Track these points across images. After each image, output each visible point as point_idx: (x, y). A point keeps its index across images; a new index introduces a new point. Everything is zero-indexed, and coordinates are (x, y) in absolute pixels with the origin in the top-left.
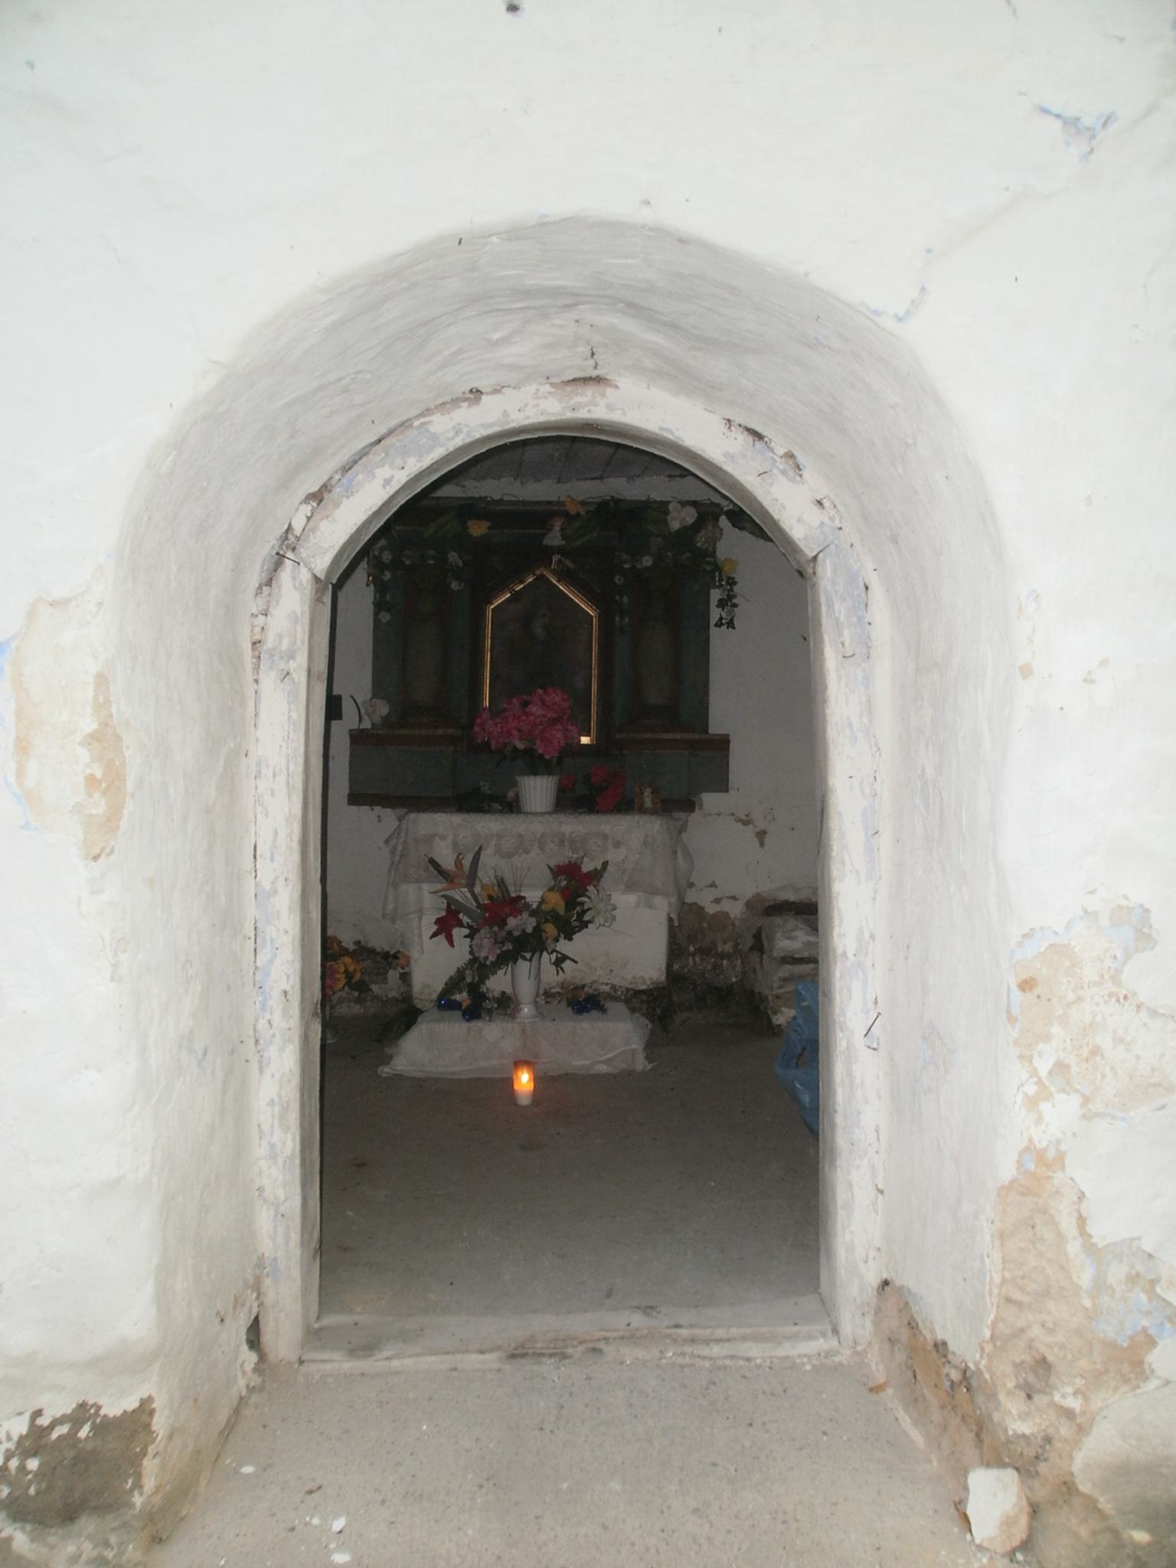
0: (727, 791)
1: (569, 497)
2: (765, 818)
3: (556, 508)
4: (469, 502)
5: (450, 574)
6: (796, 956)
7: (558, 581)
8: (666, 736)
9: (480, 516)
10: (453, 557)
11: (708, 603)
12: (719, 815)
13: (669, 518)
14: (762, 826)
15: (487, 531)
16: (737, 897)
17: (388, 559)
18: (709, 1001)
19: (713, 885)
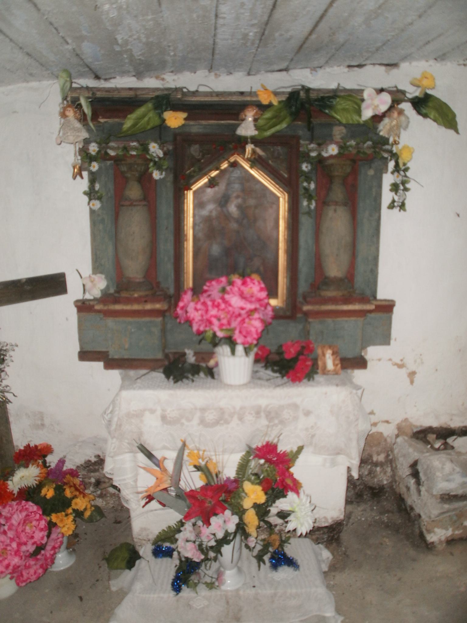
0: (389, 344)
1: (263, 86)
2: (415, 361)
3: (248, 99)
4: (166, 92)
5: (151, 164)
6: (452, 494)
7: (251, 167)
8: (346, 307)
9: (176, 107)
10: (155, 149)
11: (380, 186)
12: (380, 360)
13: (364, 105)
14: (412, 367)
15: (183, 122)
16: (390, 421)
17: (94, 151)
18: (365, 497)
19: (372, 413)
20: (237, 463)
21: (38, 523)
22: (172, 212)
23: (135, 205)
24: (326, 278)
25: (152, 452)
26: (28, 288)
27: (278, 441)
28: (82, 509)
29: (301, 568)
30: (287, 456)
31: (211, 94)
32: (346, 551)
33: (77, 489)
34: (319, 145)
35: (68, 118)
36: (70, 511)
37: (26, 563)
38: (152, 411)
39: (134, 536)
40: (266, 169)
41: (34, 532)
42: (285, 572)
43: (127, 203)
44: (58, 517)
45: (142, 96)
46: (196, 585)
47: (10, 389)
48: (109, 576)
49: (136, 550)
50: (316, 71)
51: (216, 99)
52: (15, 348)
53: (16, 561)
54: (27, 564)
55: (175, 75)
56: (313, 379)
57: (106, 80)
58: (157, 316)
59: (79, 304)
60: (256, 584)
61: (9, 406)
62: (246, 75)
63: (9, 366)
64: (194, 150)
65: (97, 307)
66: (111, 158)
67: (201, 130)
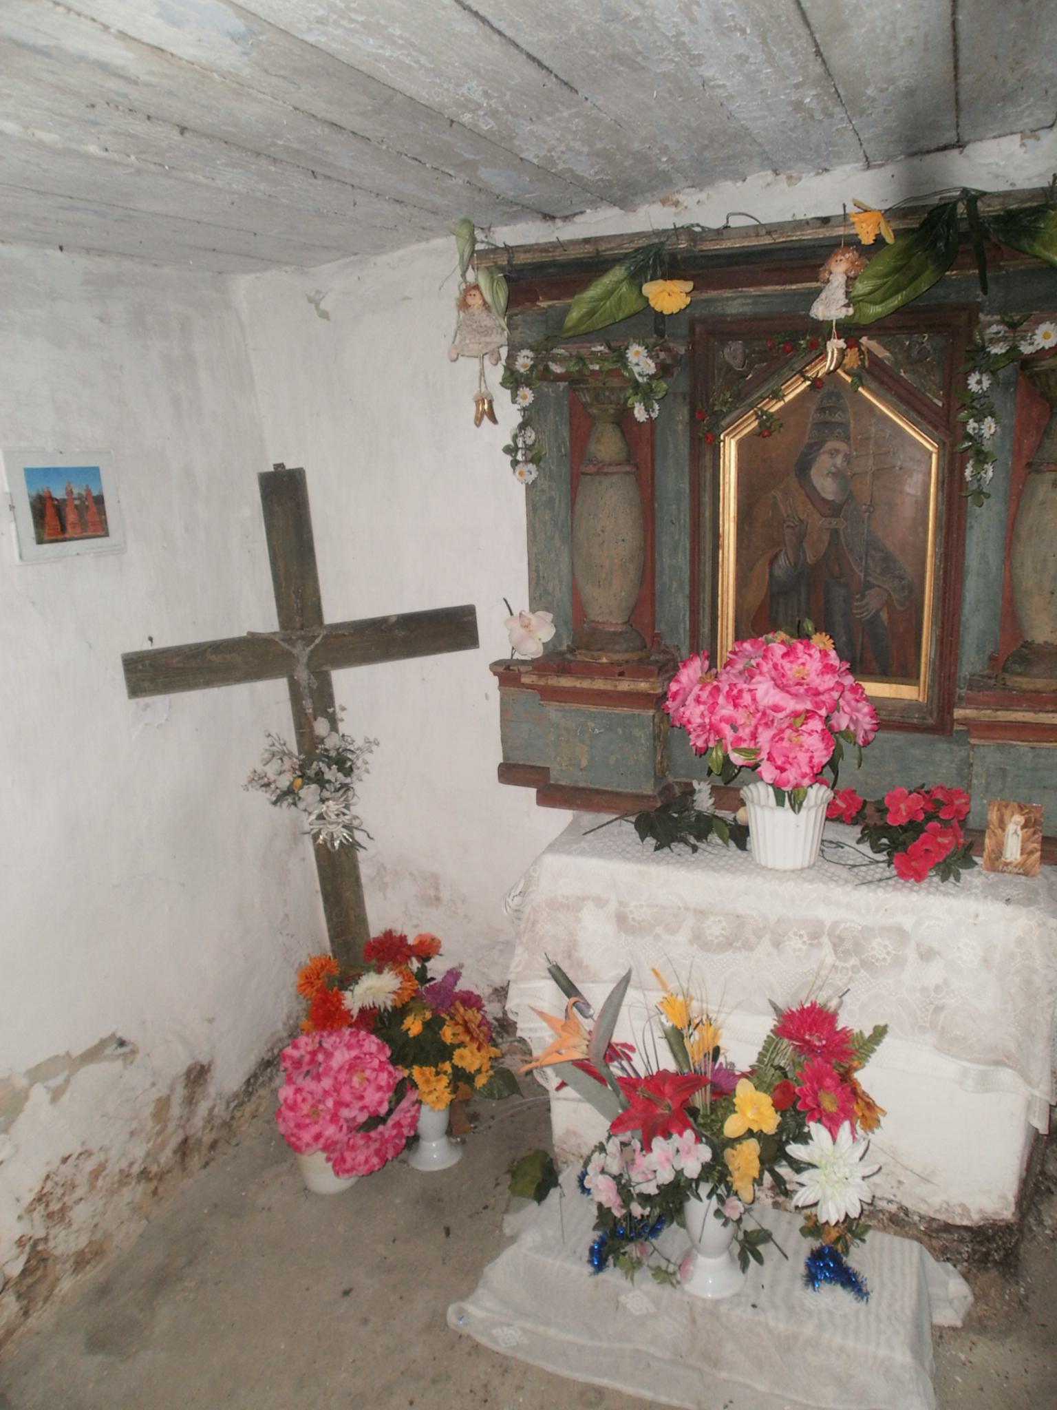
20: (765, 1038)
21: (374, 1075)
22: (686, 486)
23: (606, 474)
24: (1027, 645)
25: (578, 985)
26: (400, 633)
27: (840, 1004)
28: (472, 1069)
29: (873, 1296)
30: (848, 1042)
31: (757, 230)
32: (1027, 1297)
33: (468, 1031)
34: (1013, 326)
35: (470, 310)
36: (447, 1067)
37: (349, 1139)
38: (600, 903)
39: (554, 1142)
40: (890, 389)
41: (365, 1089)
42: (832, 1296)
43: (591, 469)
44: (423, 1074)
45: (608, 253)
46: (636, 1264)
47: (362, 823)
48: (508, 1206)
49: (555, 1168)
50: (1038, 139)
51: (767, 240)
52: (374, 748)
53: (330, 1131)
54: (351, 1142)
55: (701, 190)
56: (958, 879)
57: (566, 218)
58: (644, 707)
59: (501, 669)
60: (763, 1301)
61: (361, 855)
62: (863, 170)
63: (361, 780)
64: (733, 353)
65: (525, 680)
66: (559, 378)
67: (747, 309)
